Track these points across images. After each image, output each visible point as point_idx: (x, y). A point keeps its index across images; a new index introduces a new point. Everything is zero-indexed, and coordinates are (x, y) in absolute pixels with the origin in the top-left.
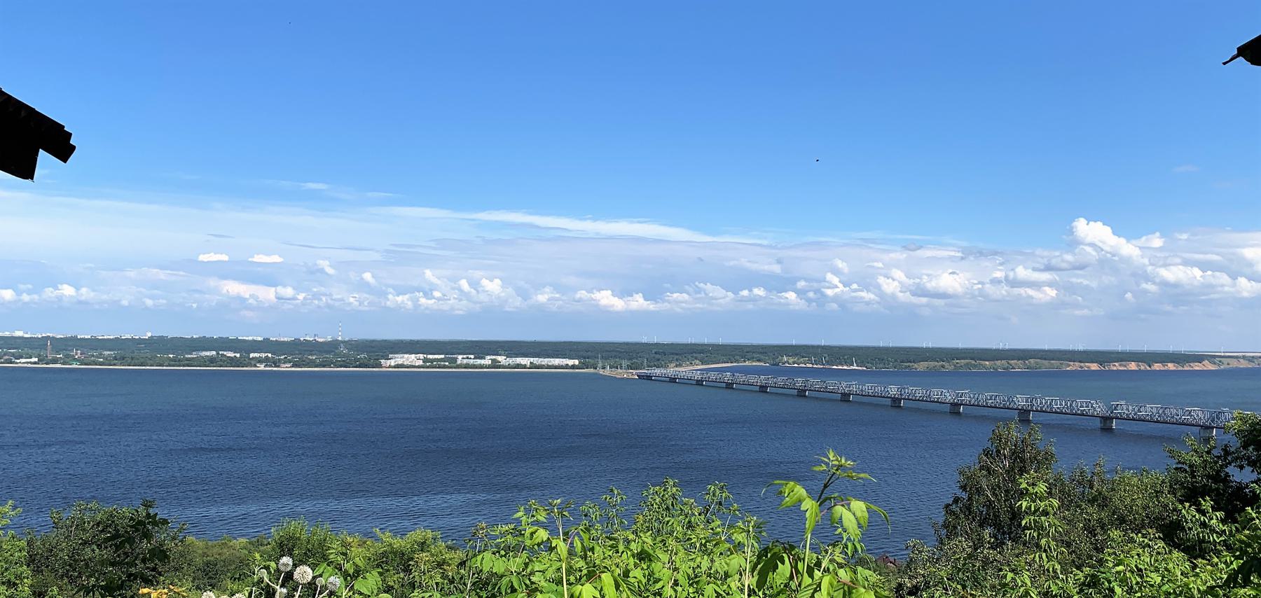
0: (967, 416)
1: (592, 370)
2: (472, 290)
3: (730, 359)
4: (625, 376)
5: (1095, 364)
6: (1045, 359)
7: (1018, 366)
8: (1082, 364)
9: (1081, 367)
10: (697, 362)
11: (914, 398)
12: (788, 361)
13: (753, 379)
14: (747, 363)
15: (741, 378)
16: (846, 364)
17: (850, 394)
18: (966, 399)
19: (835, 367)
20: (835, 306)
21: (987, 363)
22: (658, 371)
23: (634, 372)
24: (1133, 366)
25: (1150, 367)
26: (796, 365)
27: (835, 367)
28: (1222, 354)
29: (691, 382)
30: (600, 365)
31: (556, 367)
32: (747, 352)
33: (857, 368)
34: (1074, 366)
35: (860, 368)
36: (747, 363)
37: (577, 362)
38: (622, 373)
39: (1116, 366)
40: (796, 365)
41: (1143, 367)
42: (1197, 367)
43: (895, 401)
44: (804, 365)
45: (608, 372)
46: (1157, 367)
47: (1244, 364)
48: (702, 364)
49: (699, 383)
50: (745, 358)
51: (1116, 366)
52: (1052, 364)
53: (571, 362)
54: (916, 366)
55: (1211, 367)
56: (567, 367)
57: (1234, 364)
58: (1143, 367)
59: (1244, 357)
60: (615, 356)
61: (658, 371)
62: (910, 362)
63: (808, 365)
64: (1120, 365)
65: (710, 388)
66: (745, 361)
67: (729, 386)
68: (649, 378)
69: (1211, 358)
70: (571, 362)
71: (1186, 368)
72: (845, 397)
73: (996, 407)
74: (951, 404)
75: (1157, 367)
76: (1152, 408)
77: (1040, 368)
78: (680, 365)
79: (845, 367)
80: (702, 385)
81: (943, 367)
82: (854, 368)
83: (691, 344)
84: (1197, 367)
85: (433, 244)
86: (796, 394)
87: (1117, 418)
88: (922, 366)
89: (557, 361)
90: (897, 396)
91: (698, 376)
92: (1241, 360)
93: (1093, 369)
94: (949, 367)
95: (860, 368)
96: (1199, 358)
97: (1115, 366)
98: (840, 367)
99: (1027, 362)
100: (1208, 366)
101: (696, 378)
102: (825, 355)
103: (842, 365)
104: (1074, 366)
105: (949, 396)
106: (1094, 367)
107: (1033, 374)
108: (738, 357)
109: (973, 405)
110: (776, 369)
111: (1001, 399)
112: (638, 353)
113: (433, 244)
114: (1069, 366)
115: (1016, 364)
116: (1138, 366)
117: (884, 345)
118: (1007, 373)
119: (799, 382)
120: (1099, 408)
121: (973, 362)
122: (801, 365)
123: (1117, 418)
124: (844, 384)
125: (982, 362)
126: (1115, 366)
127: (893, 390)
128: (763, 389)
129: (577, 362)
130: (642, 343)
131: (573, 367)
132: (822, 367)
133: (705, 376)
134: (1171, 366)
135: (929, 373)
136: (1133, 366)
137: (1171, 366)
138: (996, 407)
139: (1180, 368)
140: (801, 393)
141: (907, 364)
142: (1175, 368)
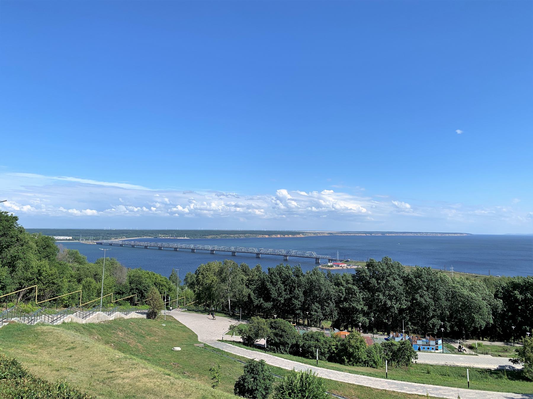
0: (263, 258)
1: (77, 241)
2: (138, 208)
3: (138, 236)
4: (91, 243)
5: (267, 236)
6: (251, 234)
7: (242, 236)
8: (263, 236)
9: (263, 237)
10: (124, 237)
11: (199, 249)
12: (162, 237)
13: (142, 244)
14: (145, 237)
15: (138, 243)
16: (183, 237)
17: (195, 249)
18: (216, 249)
19: (178, 238)
20: (177, 215)
21: (232, 235)
22: (105, 241)
23: (95, 241)
24: (279, 236)
25: (284, 236)
26: (164, 238)
27: (178, 238)
28: (308, 232)
29: (118, 245)
30: (81, 239)
31: (61, 240)
32: (145, 233)
33: (186, 238)
34: (260, 236)
35: (188, 238)
36: (145, 237)
37: (71, 238)
38: (90, 242)
39: (274, 236)
40: (164, 238)
41: (282, 236)
42: (298, 236)
43: (193, 250)
44: (167, 238)
45: (83, 242)
46: (286, 236)
47: (312, 235)
48: (126, 238)
49: (121, 245)
50: (144, 235)
51: (274, 236)
52: (253, 236)
53: (68, 238)
54: (207, 237)
55: (302, 236)
56: (66, 240)
57: (310, 235)
58: (282, 236)
59: (313, 233)
60: (90, 235)
61: (105, 241)
62: (206, 236)
63: (169, 238)
64: (275, 236)
65: (116, 246)
66: (144, 237)
67: (133, 246)
68: (101, 244)
69: (303, 233)
70: (68, 238)
71: (295, 237)
72: (176, 249)
73: (225, 251)
74: (211, 250)
75: (286, 236)
76: (308, 253)
77: (249, 237)
78: (117, 239)
79: (182, 238)
80: (123, 246)
81: (217, 237)
82: (185, 238)
83: (125, 230)
84: (298, 236)
85: (23, 189)
86: (173, 250)
87: (261, 254)
88: (209, 237)
89: (62, 238)
90: (193, 248)
91: (121, 243)
92: (312, 234)
93: (266, 237)
94: (219, 237)
95: (188, 238)
96: (299, 233)
97: (273, 236)
98: (180, 238)
99: (245, 235)
100: (302, 236)
101: (144, 245)
102: (175, 234)
103: (181, 237)
104: (260, 236)
105: (210, 248)
106: (267, 236)
107: (234, 240)
108: (141, 235)
109: (218, 251)
110: (156, 240)
111: (226, 248)
112: (100, 234)
113: (23, 189)
114: (259, 236)
115: (242, 236)
116: (280, 236)
117: (127, 228)
118: (239, 239)
119: (159, 244)
120: (256, 251)
121: (227, 235)
122: (166, 238)
123: (261, 254)
124: (175, 244)
125: (230, 235)
126: (273, 236)
127: (192, 246)
128: (146, 247)
129: (71, 238)
130: (124, 230)
131: (69, 240)
132: (173, 238)
133: (124, 243)
134: (290, 236)
135: (213, 240)
136: (279, 236)
137: (290, 236)
138: (225, 251)
139: (293, 237)
140: (160, 248)
141: (204, 236)
142: (291, 237)
